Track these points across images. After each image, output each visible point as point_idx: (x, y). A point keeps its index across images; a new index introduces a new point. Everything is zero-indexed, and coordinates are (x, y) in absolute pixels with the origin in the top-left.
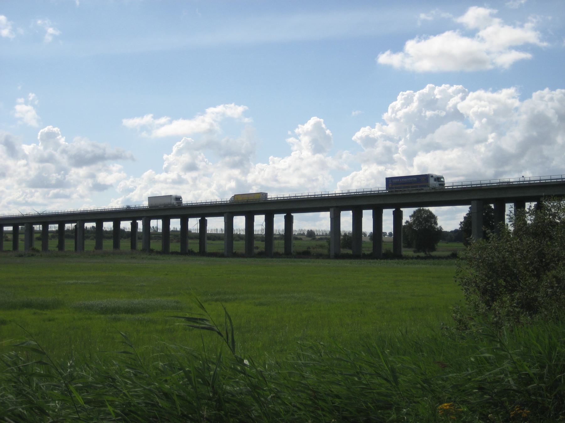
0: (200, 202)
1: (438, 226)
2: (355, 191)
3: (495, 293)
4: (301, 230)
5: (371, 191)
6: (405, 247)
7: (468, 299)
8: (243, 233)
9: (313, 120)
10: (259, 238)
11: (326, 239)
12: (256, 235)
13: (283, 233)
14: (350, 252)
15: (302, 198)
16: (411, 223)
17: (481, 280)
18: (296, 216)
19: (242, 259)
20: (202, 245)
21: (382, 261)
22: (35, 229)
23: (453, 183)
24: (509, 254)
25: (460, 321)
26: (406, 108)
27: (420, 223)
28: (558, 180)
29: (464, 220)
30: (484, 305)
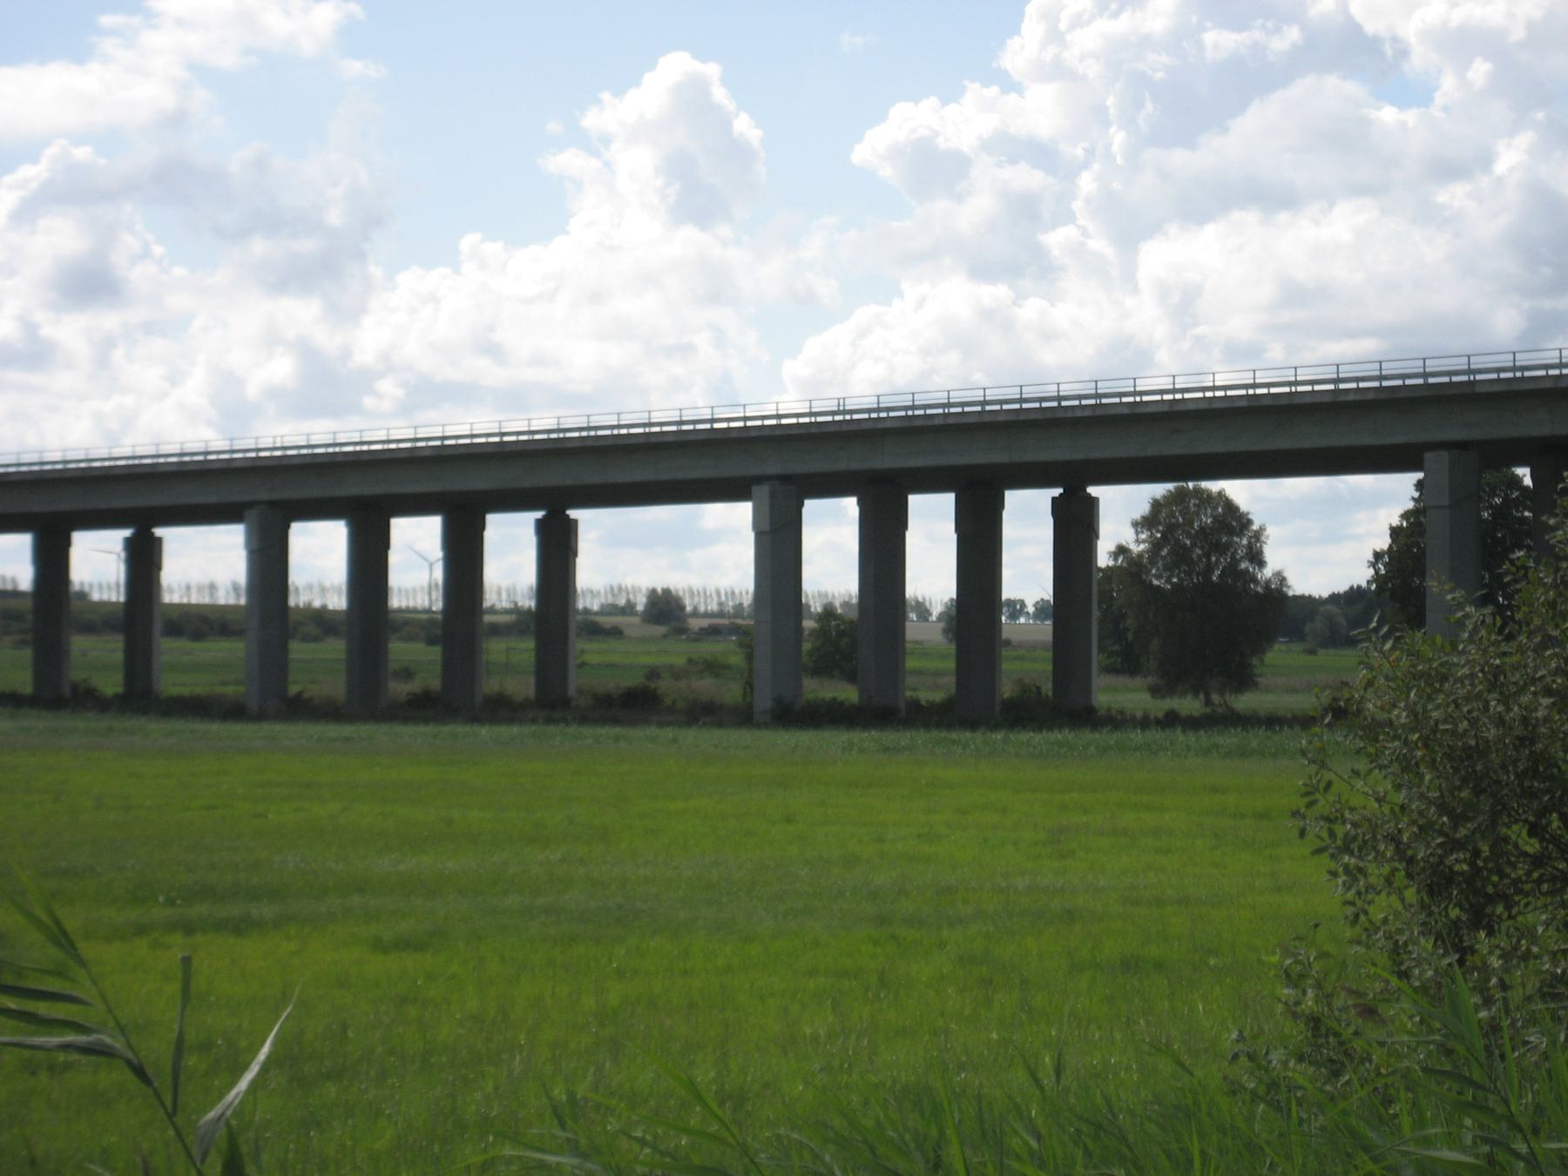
0: (127, 451)
1: (1268, 572)
2: (871, 402)
3: (1490, 890)
4: (620, 588)
5: (949, 405)
6: (1110, 670)
7: (1362, 917)
8: (338, 602)
9: (675, 66)
10: (413, 624)
11: (735, 630)
12: (400, 610)
13: (529, 603)
14: (849, 694)
15: (619, 435)
16: (1140, 555)
17: (1421, 828)
18: (592, 524)
19: (332, 730)
20: (138, 660)
21: (999, 736)
24: (1554, 704)
25: (1315, 1022)
26: (1115, 15)
27: (1181, 557)
29: (1389, 541)
30: (1427, 944)
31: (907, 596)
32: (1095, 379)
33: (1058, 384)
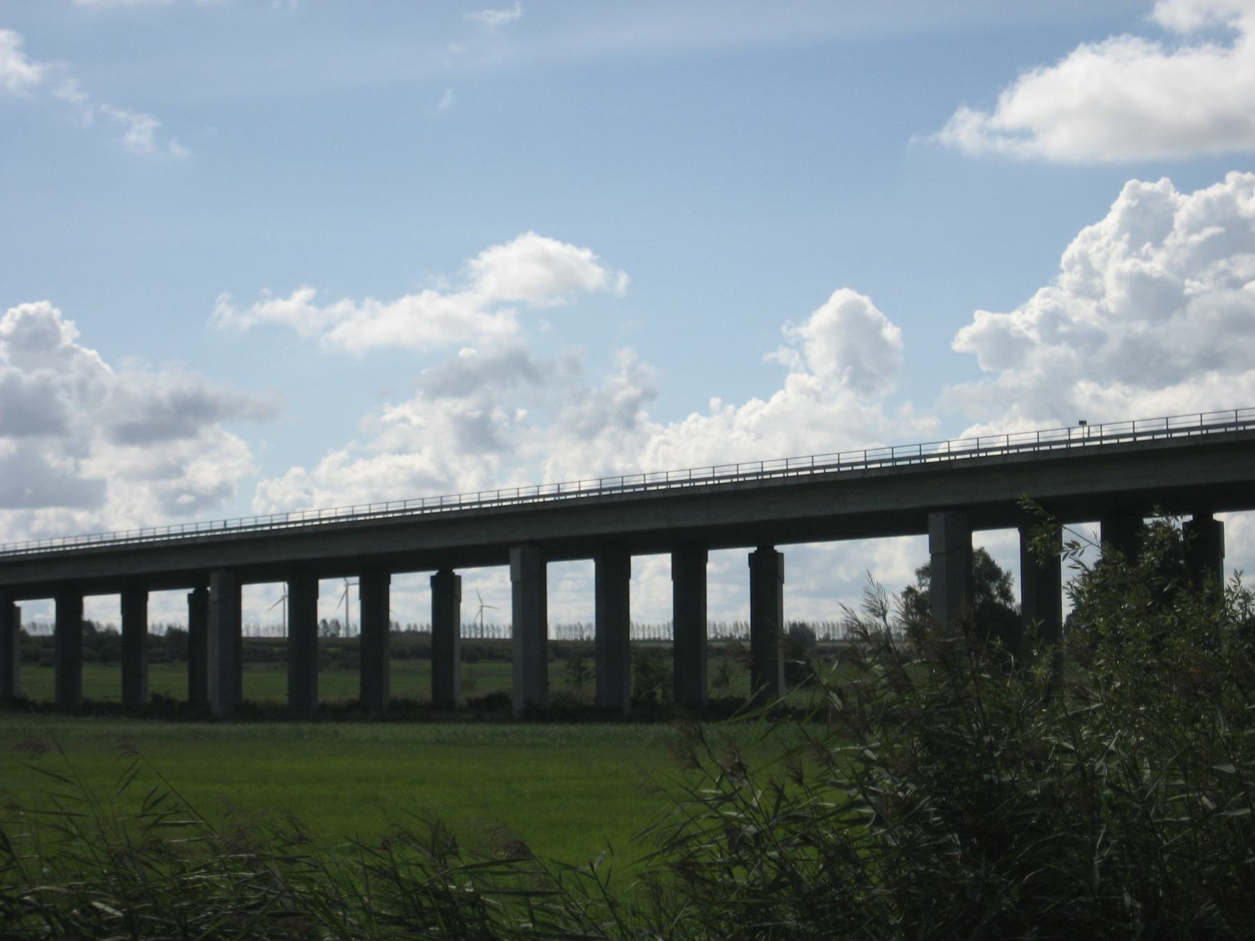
16: (923, 595)
22: (25, 621)
23: (405, 501)
28: (1121, 440)
31: (150, 623)
32: (1166, 416)
33: (667, 473)
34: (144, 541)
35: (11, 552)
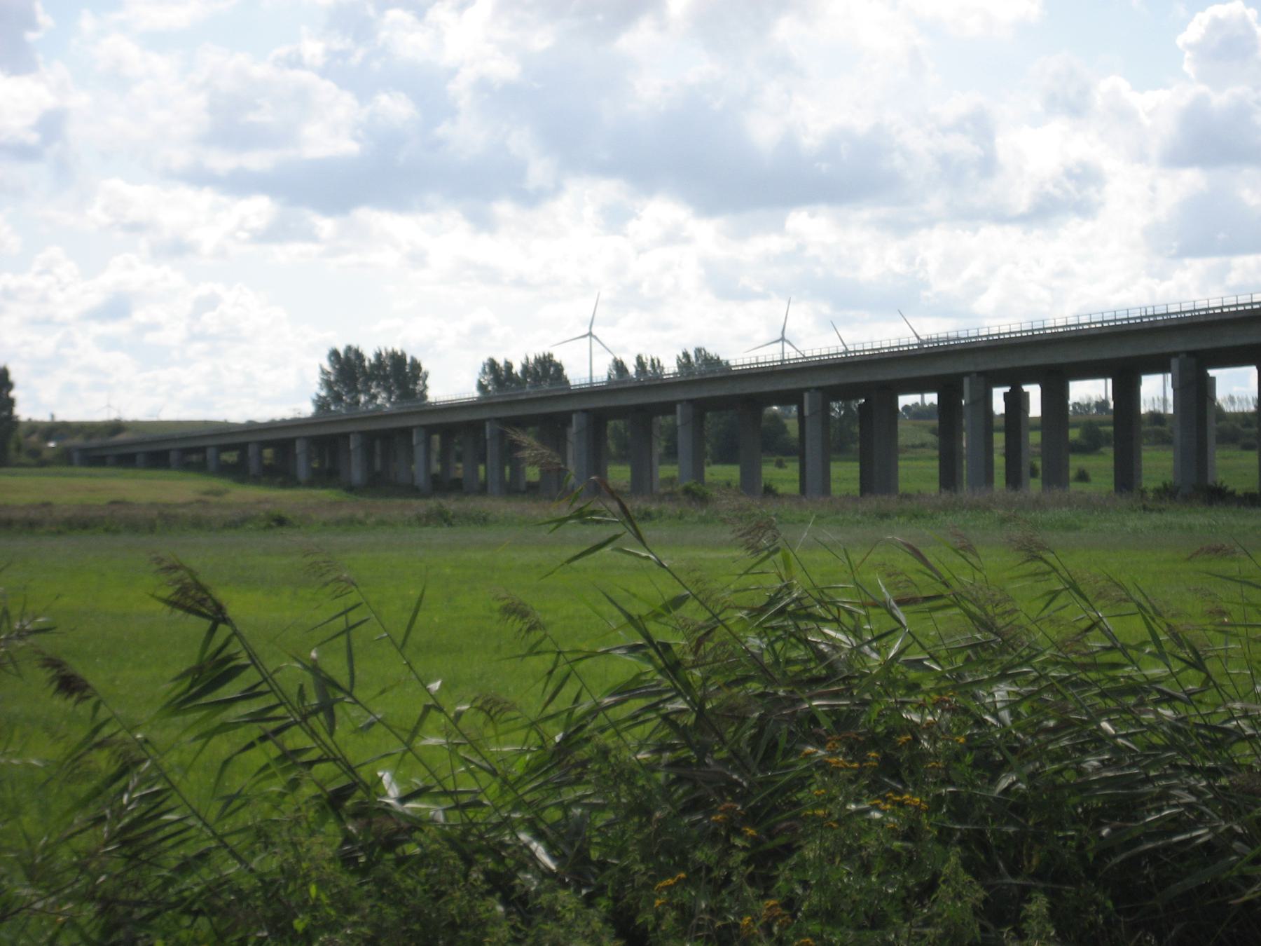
22: (1221, 394)
34: (1093, 326)
35: (974, 337)
